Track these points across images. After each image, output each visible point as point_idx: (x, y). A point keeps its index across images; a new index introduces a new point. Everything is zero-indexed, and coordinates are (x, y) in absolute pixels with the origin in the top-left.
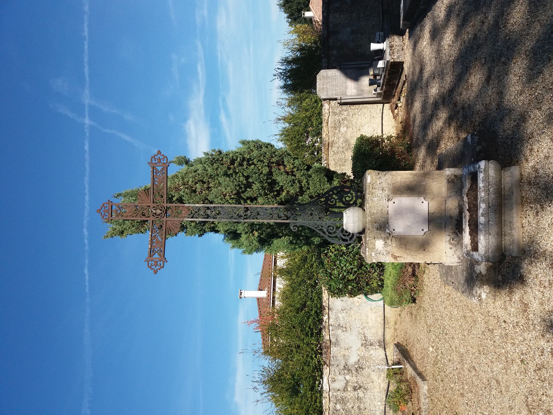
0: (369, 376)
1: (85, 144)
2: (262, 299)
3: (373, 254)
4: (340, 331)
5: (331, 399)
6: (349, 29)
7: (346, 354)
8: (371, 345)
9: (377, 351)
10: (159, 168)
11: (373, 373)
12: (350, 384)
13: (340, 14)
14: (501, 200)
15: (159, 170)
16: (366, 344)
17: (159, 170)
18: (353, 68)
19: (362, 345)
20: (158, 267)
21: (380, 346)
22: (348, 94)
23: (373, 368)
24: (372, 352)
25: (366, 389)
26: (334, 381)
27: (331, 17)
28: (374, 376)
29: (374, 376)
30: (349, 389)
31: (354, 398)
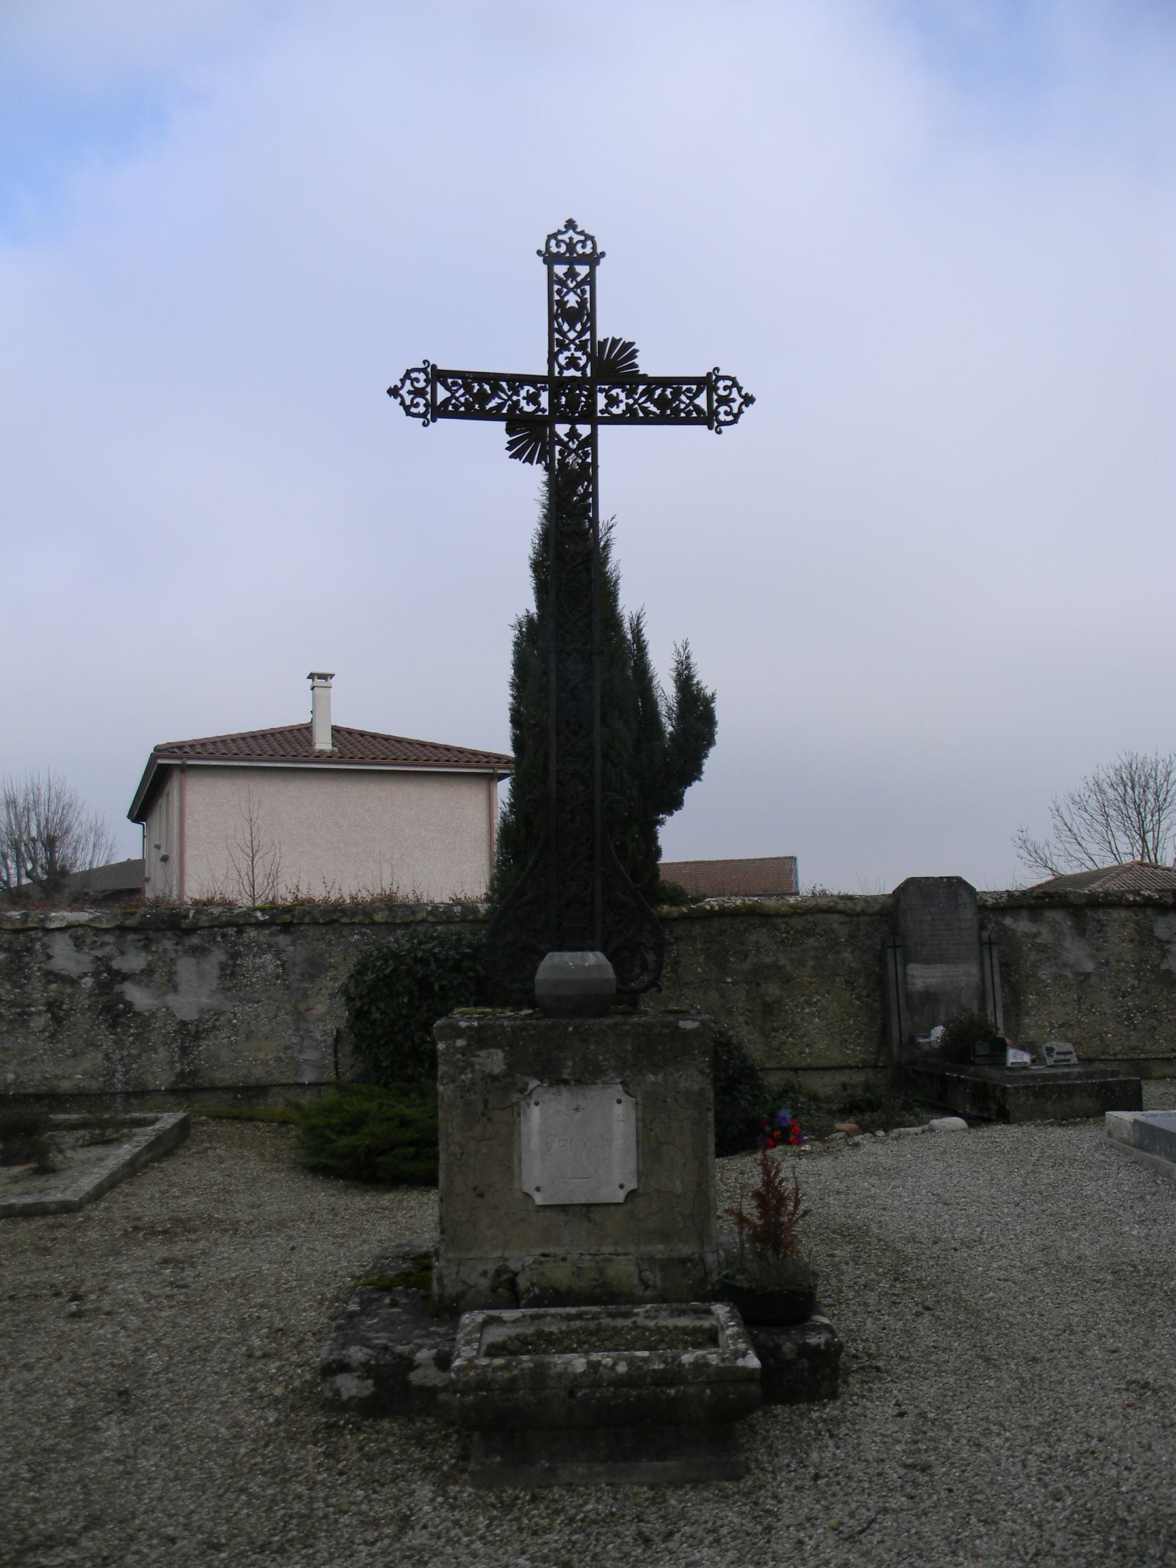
0: (93, 1044)
1: (78, 1112)
2: (310, 742)
3: (460, 1043)
4: (223, 958)
5: (22, 938)
6: (1090, 966)
7: (156, 976)
8: (184, 1051)
9: (166, 1067)
10: (702, 401)
11: (100, 1055)
12: (69, 990)
13: (1132, 941)
14: (1022, 907)
15: (696, 401)
16: (189, 1034)
17: (696, 401)
18: (983, 979)
19: (183, 1024)
20: (565, 237)
21: (182, 1075)
22: (911, 966)
23: (116, 1056)
24: (163, 1053)
25: (52, 1036)
26: (78, 943)
27: (1123, 914)
28: (92, 1060)
29: (92, 1060)
30: (54, 986)
31: (27, 1002)
